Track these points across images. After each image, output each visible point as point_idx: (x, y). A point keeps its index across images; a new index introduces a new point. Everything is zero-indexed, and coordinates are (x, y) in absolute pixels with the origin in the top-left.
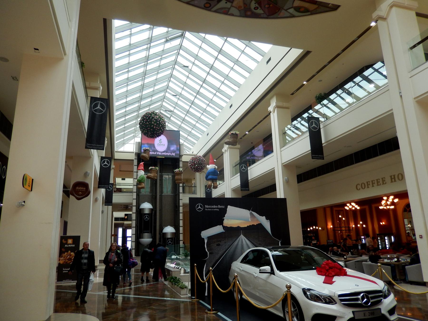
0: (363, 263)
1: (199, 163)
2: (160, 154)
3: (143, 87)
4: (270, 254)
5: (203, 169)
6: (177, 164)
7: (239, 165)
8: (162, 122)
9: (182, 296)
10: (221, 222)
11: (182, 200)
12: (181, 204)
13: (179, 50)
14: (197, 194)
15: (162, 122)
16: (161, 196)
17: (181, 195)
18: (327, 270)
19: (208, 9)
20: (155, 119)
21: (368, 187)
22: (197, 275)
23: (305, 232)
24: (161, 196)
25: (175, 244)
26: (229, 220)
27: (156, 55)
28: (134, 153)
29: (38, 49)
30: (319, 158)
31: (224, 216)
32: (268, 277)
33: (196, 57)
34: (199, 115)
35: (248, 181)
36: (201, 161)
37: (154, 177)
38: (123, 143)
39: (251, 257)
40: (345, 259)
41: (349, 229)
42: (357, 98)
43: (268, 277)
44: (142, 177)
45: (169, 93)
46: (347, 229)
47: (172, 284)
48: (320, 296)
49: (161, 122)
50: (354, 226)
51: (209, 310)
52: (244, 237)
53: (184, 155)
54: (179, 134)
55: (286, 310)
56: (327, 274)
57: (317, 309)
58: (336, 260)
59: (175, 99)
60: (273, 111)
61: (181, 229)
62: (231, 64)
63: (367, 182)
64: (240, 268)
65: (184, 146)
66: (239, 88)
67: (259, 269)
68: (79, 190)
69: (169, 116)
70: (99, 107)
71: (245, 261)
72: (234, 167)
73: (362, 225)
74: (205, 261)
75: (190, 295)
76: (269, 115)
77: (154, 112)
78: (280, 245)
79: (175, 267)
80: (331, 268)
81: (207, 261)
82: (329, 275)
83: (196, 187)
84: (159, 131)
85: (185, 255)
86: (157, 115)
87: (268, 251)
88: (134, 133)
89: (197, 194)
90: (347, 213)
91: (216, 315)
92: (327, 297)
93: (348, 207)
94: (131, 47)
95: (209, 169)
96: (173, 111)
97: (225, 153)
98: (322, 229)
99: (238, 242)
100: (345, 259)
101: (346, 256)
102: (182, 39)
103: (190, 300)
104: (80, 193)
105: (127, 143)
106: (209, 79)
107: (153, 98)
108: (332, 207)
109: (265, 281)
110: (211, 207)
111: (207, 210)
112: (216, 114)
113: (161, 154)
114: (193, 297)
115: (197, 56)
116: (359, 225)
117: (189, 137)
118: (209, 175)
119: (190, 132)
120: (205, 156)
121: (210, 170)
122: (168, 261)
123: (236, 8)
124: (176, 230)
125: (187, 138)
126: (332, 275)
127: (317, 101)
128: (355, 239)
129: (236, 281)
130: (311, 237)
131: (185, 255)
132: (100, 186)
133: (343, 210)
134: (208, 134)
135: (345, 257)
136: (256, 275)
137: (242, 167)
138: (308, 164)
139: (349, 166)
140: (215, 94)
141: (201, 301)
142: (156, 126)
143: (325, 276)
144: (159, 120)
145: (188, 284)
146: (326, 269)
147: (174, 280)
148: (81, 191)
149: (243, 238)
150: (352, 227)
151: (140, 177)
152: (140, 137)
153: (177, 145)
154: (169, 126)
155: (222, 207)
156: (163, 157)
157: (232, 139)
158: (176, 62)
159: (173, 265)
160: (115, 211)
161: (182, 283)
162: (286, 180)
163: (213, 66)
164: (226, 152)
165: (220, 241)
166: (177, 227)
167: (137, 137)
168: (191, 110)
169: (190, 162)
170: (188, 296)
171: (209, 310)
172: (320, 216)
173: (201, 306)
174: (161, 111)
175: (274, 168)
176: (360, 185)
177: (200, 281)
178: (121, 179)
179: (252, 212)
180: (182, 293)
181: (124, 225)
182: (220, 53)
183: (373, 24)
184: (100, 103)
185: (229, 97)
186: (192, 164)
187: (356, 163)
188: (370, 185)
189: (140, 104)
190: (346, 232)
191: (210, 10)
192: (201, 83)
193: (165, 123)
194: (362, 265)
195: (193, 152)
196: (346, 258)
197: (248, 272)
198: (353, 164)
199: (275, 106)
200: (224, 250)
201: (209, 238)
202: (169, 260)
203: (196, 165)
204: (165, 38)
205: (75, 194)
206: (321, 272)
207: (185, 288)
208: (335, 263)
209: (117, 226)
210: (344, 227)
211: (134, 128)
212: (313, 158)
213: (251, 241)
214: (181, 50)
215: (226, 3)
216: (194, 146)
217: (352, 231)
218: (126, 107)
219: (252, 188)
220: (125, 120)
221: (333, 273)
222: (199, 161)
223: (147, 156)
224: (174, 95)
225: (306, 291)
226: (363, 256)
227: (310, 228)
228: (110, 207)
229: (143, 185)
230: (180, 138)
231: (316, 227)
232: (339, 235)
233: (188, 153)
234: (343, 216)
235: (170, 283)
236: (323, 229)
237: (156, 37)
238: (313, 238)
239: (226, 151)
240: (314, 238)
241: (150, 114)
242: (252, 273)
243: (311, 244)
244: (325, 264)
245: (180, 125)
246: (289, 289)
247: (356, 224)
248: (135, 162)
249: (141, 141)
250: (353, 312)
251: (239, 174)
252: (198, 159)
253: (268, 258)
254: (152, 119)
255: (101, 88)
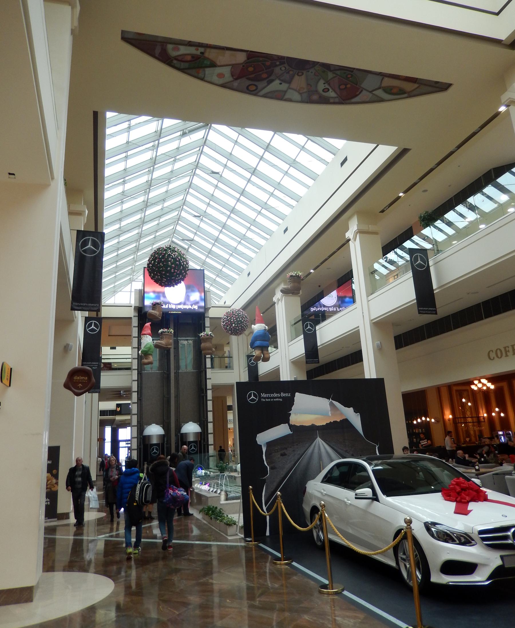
0: (507, 477)
1: (239, 321)
2: (174, 307)
3: (146, 205)
4: (369, 468)
5: (245, 330)
6: (201, 322)
7: (301, 321)
8: (184, 261)
9: (229, 538)
10: (286, 419)
11: (210, 379)
12: (209, 386)
13: (202, 147)
14: (233, 369)
15: (184, 261)
16: (177, 374)
17: (209, 371)
18: (459, 493)
19: (252, 92)
20: (172, 258)
21: (507, 356)
22: (253, 502)
23: (410, 426)
24: (177, 374)
25: (201, 452)
26: (298, 414)
27: (167, 156)
28: (133, 308)
29: (14, 174)
30: (429, 312)
31: (291, 410)
32: (369, 505)
33: (230, 157)
34: (234, 244)
35: (317, 347)
36: (240, 318)
37: (166, 346)
38: (114, 292)
39: (336, 473)
40: (476, 470)
41: (478, 421)
42: (482, 214)
43: (369, 505)
44: (148, 346)
45: (187, 212)
46: (475, 420)
47: (211, 519)
48: (451, 534)
49: (181, 262)
50: (485, 415)
51: (279, 559)
52: (323, 442)
53: (212, 307)
54: (204, 274)
55: (399, 555)
56: (458, 499)
57: (449, 553)
58: (463, 472)
59: (196, 221)
60: (353, 239)
61: (210, 426)
62: (285, 167)
63: (505, 348)
64: (322, 491)
65: (211, 293)
66: (298, 202)
67: (355, 493)
68: (78, 381)
69: (186, 247)
70: (90, 246)
71: (328, 479)
72: (292, 325)
73: (499, 413)
74: (264, 481)
75: (243, 536)
76: (347, 243)
77: (170, 246)
78: (378, 454)
79: (209, 490)
80: (464, 489)
81: (267, 481)
82: (462, 500)
83: (232, 357)
84: (179, 276)
85: (220, 468)
86: (176, 251)
87: (365, 464)
88: (131, 275)
89: (233, 369)
90: (473, 395)
91: (290, 567)
92: (462, 534)
93: (476, 385)
94: (129, 145)
95: (255, 331)
96: (192, 240)
97: (278, 304)
98: (436, 421)
99: (313, 450)
100: (476, 470)
101: (478, 466)
102: (208, 130)
103: (243, 544)
104: (80, 385)
105: (120, 291)
106: (251, 189)
107: (162, 220)
108: (449, 387)
109: (365, 512)
110: (270, 395)
111: (264, 400)
112: (262, 242)
113: (176, 307)
114: (248, 539)
115: (230, 154)
116: (494, 414)
117: (218, 279)
118: (256, 341)
119: (220, 270)
120: (245, 307)
121: (257, 332)
122: (196, 480)
123: (295, 90)
124: (201, 428)
125: (215, 280)
126: (466, 500)
127: (422, 224)
128: (489, 436)
129: (323, 513)
130: (419, 434)
131: (220, 468)
132: (84, 363)
133: (467, 390)
134: (249, 274)
135: (477, 467)
136: (349, 502)
137: (307, 326)
138: (411, 320)
139: (475, 322)
140: (260, 212)
141: (261, 545)
142: (175, 268)
143: (455, 503)
144: (179, 259)
145: (238, 518)
146: (457, 491)
147: (213, 512)
148: (81, 383)
149: (320, 443)
150: (483, 417)
151: (145, 346)
152: (142, 281)
153: (200, 292)
154: (192, 265)
155: (287, 395)
156: (179, 312)
157: (292, 285)
158: (197, 165)
159: (205, 487)
160: (101, 401)
161: (227, 516)
162: (378, 346)
163: (256, 170)
164: (280, 302)
165: (286, 449)
166: (203, 424)
167: (136, 280)
168: (222, 237)
169: (224, 319)
170: (238, 537)
171: (279, 559)
172: (432, 401)
173: (263, 553)
174: (174, 239)
175: (358, 327)
176: (494, 351)
177: (261, 514)
178: (110, 347)
179: (333, 401)
180: (229, 533)
181: (116, 421)
182: (267, 150)
183: (502, 109)
184: (91, 238)
185: (283, 217)
186: (226, 323)
187: (486, 318)
188: (509, 352)
189: (142, 230)
190: (473, 426)
191: (256, 95)
192: (238, 195)
193: (187, 264)
194: (505, 480)
195: (225, 303)
196: (479, 469)
197: (335, 498)
198: (482, 319)
199: (356, 230)
200: (293, 463)
201: (269, 444)
202: (197, 479)
203: (234, 325)
204: (181, 131)
205: (74, 388)
206: (450, 496)
207: (233, 525)
208: (469, 483)
209: (103, 424)
210: (470, 417)
211: (131, 267)
212: (419, 313)
213: (333, 446)
214: (205, 146)
215: (281, 84)
216: (226, 292)
217: (483, 423)
218: (119, 236)
219: (324, 357)
220: (117, 255)
221: (468, 498)
222: (237, 318)
223: (158, 313)
224: (195, 216)
225: (430, 525)
226: (503, 465)
227: (417, 421)
228: (96, 396)
229: (151, 359)
230: (204, 280)
231: (426, 419)
232: (462, 429)
233: (217, 303)
234: (468, 400)
235: (207, 517)
236: (437, 421)
237: (168, 129)
238: (421, 437)
239: (279, 300)
240: (423, 437)
241: (165, 250)
242: (342, 500)
243: (419, 446)
244: (455, 483)
245: (205, 261)
246: (409, 525)
247: (489, 412)
248: (135, 322)
249: (143, 288)
250: (502, 557)
251: (302, 336)
252: (236, 314)
253: (363, 474)
254: (168, 258)
255: (87, 212)
